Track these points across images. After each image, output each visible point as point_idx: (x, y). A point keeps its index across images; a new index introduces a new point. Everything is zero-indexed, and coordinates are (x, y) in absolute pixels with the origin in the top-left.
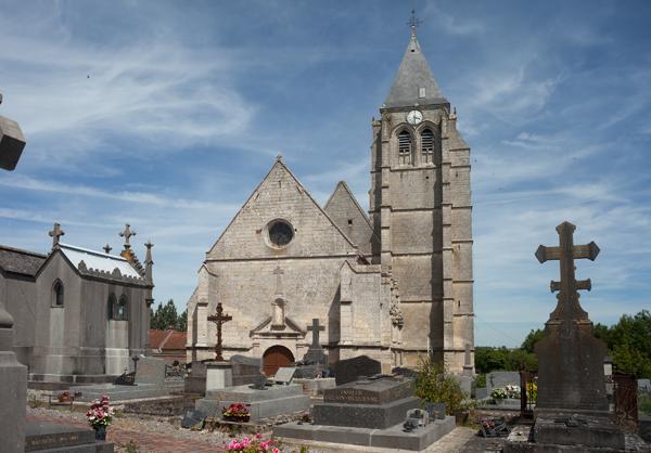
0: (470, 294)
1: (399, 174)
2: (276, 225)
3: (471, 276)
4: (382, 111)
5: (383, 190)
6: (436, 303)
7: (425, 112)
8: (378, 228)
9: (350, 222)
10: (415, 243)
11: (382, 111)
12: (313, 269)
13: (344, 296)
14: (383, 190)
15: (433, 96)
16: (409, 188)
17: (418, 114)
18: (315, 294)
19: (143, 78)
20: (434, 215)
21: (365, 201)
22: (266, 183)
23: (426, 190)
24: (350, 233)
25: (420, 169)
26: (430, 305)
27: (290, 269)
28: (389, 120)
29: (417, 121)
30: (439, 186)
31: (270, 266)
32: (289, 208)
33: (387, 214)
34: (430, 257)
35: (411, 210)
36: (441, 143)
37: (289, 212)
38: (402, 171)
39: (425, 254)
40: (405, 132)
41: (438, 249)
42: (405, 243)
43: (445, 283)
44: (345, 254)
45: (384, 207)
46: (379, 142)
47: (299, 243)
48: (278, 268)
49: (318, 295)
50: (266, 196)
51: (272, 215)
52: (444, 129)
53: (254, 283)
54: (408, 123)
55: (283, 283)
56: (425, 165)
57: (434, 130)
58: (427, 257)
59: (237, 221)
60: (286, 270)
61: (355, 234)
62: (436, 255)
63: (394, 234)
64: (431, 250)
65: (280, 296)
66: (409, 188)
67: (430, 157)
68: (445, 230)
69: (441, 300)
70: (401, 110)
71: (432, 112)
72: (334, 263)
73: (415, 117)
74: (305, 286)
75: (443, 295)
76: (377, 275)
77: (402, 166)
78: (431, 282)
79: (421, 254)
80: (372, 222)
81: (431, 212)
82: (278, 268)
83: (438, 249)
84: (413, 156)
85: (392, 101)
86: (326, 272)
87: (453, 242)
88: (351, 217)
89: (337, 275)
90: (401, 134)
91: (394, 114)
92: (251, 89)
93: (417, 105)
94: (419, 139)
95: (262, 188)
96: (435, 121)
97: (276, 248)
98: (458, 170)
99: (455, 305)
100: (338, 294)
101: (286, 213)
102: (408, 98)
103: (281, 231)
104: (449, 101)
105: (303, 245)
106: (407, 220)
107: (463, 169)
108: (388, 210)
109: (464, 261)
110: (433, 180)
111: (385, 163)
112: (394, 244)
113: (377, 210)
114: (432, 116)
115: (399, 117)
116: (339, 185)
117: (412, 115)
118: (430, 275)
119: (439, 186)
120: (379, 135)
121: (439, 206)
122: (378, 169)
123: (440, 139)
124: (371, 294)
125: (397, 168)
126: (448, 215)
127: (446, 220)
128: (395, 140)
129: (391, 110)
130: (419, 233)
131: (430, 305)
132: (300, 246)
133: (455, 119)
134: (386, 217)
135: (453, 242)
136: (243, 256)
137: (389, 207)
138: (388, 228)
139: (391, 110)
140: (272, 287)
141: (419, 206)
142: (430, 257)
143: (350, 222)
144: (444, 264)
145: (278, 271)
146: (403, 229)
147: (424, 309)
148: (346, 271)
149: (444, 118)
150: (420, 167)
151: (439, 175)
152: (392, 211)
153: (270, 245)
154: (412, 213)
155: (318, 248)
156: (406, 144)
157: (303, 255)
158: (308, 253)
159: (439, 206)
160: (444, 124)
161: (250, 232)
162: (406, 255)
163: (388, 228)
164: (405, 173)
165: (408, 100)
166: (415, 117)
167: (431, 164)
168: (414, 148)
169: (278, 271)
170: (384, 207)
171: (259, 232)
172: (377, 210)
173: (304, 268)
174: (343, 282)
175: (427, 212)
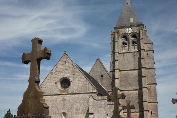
0: (156, 109)
1: (122, 54)
2: (63, 79)
3: (156, 100)
4: (115, 28)
5: (116, 62)
6: (141, 113)
7: (133, 28)
8: (114, 79)
9: (102, 76)
10: (130, 85)
11: (115, 28)
12: (78, 99)
13: (90, 111)
14: (116, 62)
15: (136, 21)
16: (127, 60)
17: (130, 29)
18: (79, 110)
19: (45, 18)
20: (138, 72)
21: (108, 67)
22: (60, 62)
23: (135, 62)
24: (102, 81)
25: (132, 52)
26: (138, 113)
27: (69, 99)
28: (118, 32)
29: (130, 32)
30: (140, 59)
31: (60, 98)
32: (69, 73)
33: (118, 72)
34: (138, 91)
35: (128, 70)
36: (140, 41)
37: (69, 74)
38: (123, 53)
39: (135, 90)
40: (125, 37)
41: (141, 89)
42: (126, 85)
43: (144, 103)
44: (92, 92)
45: (116, 69)
46: (114, 41)
47: (73, 87)
48: (64, 98)
49: (80, 110)
50: (59, 67)
51: (62, 76)
52: (141, 35)
53: (53, 105)
54: (126, 33)
55: (65, 105)
56: (134, 50)
57: (137, 35)
58: (136, 91)
59: (47, 79)
60: (67, 99)
61: (104, 81)
62: (140, 90)
63: (121, 81)
64: (138, 88)
65: (64, 111)
66: (127, 60)
67: (136, 47)
68: (143, 79)
69: (143, 111)
70: (123, 27)
71: (136, 28)
72: (87, 95)
73: (129, 30)
74: (75, 107)
75: (143, 109)
76: (105, 101)
77: (125, 51)
78: (138, 103)
79: (133, 90)
80: (111, 76)
81: (137, 71)
82: (64, 98)
83: (141, 89)
84: (129, 47)
85: (119, 24)
86: (84, 100)
87: (147, 84)
88: (102, 74)
89: (88, 101)
90: (123, 37)
91: (120, 30)
92: (88, 20)
93: (129, 25)
94: (131, 40)
95: (58, 64)
96: (137, 32)
97: (63, 90)
98: (148, 52)
99: (149, 114)
100: (88, 110)
101: (67, 74)
102: (126, 23)
103: (65, 82)
104: (143, 23)
105: (74, 88)
106: (127, 75)
107: (150, 52)
108: (118, 71)
109: (153, 92)
110: (137, 57)
111: (116, 50)
112: (121, 86)
113: (113, 71)
114: (136, 30)
115: (122, 31)
116: (97, 60)
117: (127, 29)
118: (138, 100)
119: (140, 59)
120: (114, 38)
121: (140, 69)
122: (114, 53)
123: (140, 39)
124: (103, 109)
125: (122, 52)
126: (144, 72)
127: (143, 75)
128: (120, 40)
129: (118, 28)
130: (132, 80)
131: (138, 113)
132: (73, 89)
133: (146, 31)
134: (117, 74)
135: (147, 84)
136: (49, 93)
137: (118, 69)
138: (118, 79)
139: (118, 28)
140: (61, 107)
141: (132, 68)
142: (138, 91)
143: (102, 76)
144: (143, 94)
145: (64, 100)
146: (125, 79)
147: (136, 115)
148: (91, 100)
149: (141, 30)
150: (131, 51)
151: (140, 55)
152: (120, 71)
153: (60, 88)
154: (129, 71)
155: (81, 89)
156: (125, 42)
157: (74, 93)
158: (77, 92)
159: (140, 69)
160: (141, 33)
161: (53, 83)
162: (127, 90)
163: (118, 79)
164: (125, 54)
165: (125, 23)
166: (129, 30)
167: (136, 50)
168: (129, 43)
169: (64, 100)
170: (116, 69)
171: (56, 83)
172: (113, 71)
173: (74, 98)
174: (90, 106)
175: (135, 71)
